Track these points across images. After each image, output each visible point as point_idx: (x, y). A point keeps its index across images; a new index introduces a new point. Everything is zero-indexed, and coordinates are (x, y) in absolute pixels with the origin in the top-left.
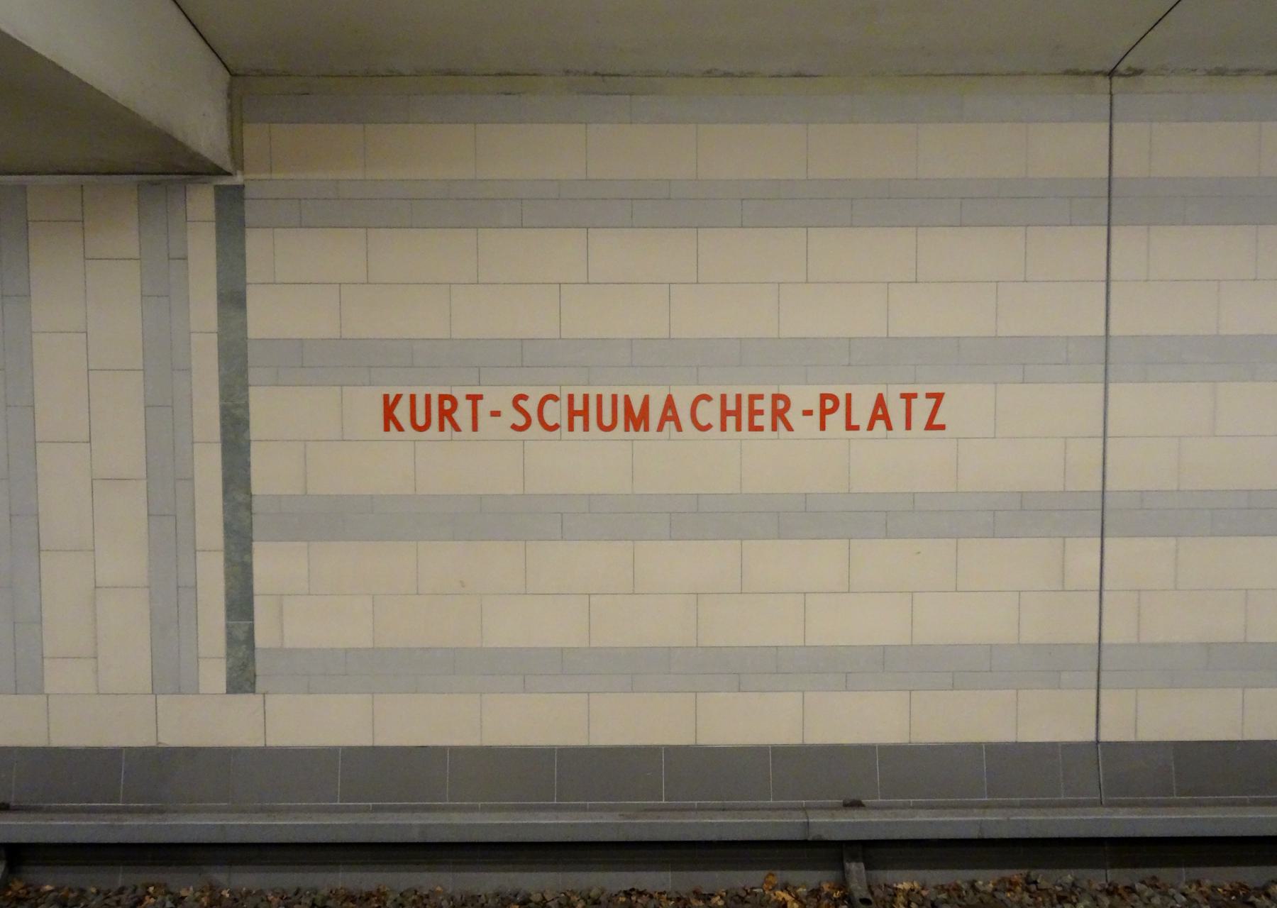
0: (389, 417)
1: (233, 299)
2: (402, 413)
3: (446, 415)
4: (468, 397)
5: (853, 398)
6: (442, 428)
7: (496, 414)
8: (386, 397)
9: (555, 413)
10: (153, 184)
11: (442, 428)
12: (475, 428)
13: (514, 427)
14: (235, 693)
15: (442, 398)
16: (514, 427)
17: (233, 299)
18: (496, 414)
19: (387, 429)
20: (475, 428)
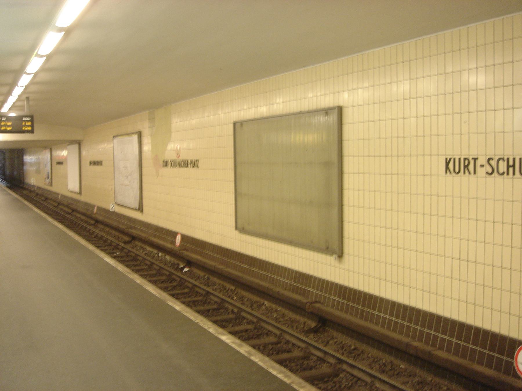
0: (447, 167)
1: (403, 86)
2: (451, 166)
3: (466, 167)
4: (473, 159)
5: (190, 171)
6: (464, 173)
7: (482, 166)
8: (446, 159)
9: (503, 166)
10: (18, 200)
11: (464, 173)
12: (475, 173)
13: (487, 173)
14: (503, 339)
15: (465, 159)
16: (487, 173)
17: (403, 86)
18: (482, 166)
19: (446, 172)
20: (475, 173)
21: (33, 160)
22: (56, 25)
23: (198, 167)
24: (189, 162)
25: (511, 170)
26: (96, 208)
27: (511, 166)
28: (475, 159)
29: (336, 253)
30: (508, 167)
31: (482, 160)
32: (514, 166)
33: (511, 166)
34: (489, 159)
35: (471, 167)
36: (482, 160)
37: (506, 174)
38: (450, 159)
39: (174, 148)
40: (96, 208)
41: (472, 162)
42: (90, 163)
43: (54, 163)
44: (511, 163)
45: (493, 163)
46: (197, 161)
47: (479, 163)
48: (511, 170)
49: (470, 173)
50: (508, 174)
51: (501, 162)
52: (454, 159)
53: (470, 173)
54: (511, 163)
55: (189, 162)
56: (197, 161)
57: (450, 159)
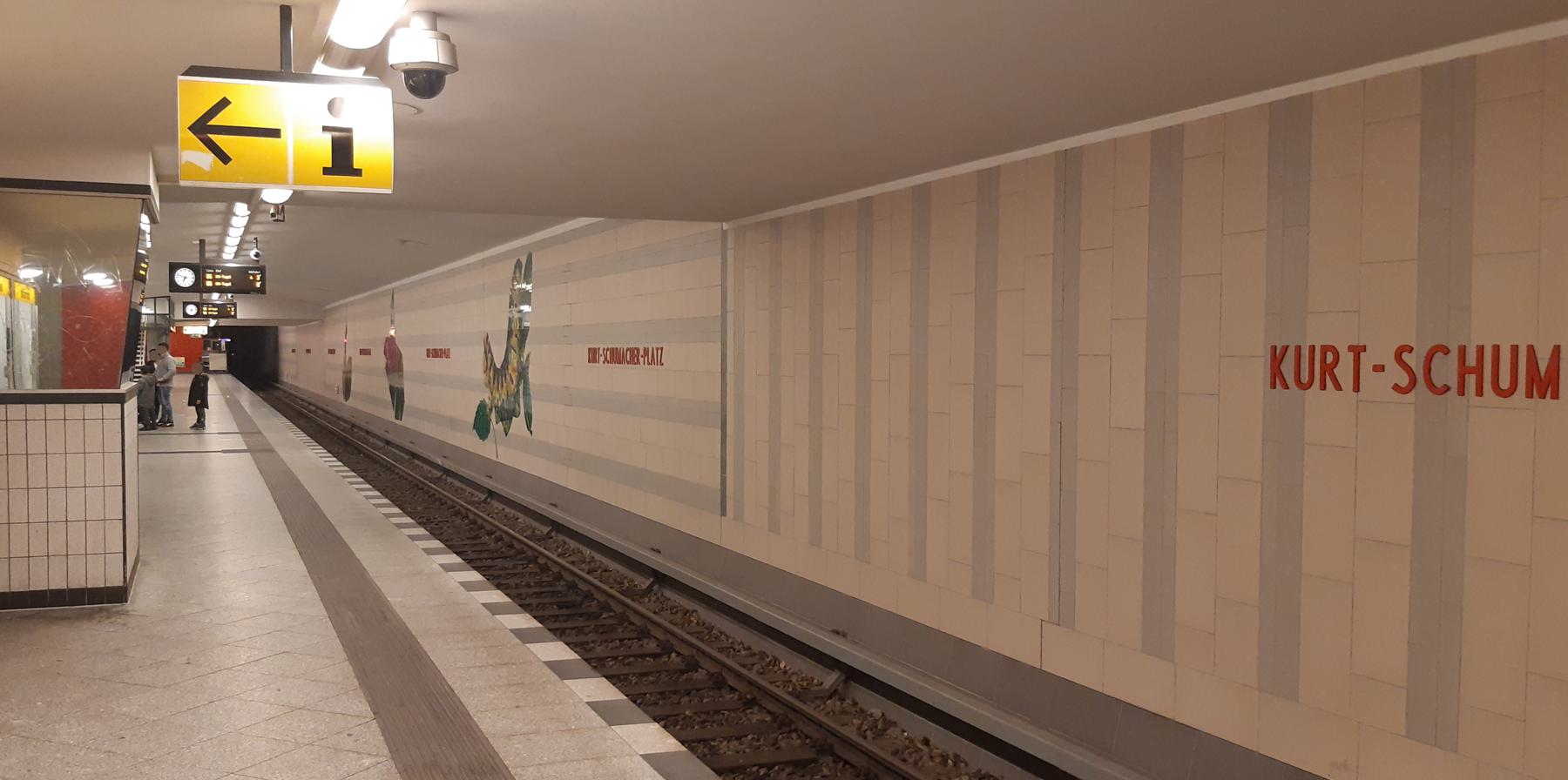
2: (1288, 368)
3: (1329, 370)
4: (1351, 348)
6: (1323, 387)
7: (1379, 368)
9: (1445, 372)
12: (1357, 388)
13: (1396, 388)
15: (1325, 349)
16: (1396, 388)
18: (1379, 368)
19: (1273, 386)
20: (1357, 388)
22: (391, 62)
25: (1471, 380)
27: (1471, 371)
28: (1357, 351)
29: (362, 64)
30: (1463, 371)
31: (1380, 352)
33: (1471, 371)
35: (1344, 372)
36: (1380, 352)
38: (1286, 348)
39: (213, 387)
41: (1347, 359)
42: (593, 355)
44: (1471, 361)
47: (1367, 361)
48: (1471, 380)
49: (1338, 387)
50: (1462, 392)
52: (1298, 349)
53: (1338, 387)
54: (1471, 361)
57: (1286, 348)
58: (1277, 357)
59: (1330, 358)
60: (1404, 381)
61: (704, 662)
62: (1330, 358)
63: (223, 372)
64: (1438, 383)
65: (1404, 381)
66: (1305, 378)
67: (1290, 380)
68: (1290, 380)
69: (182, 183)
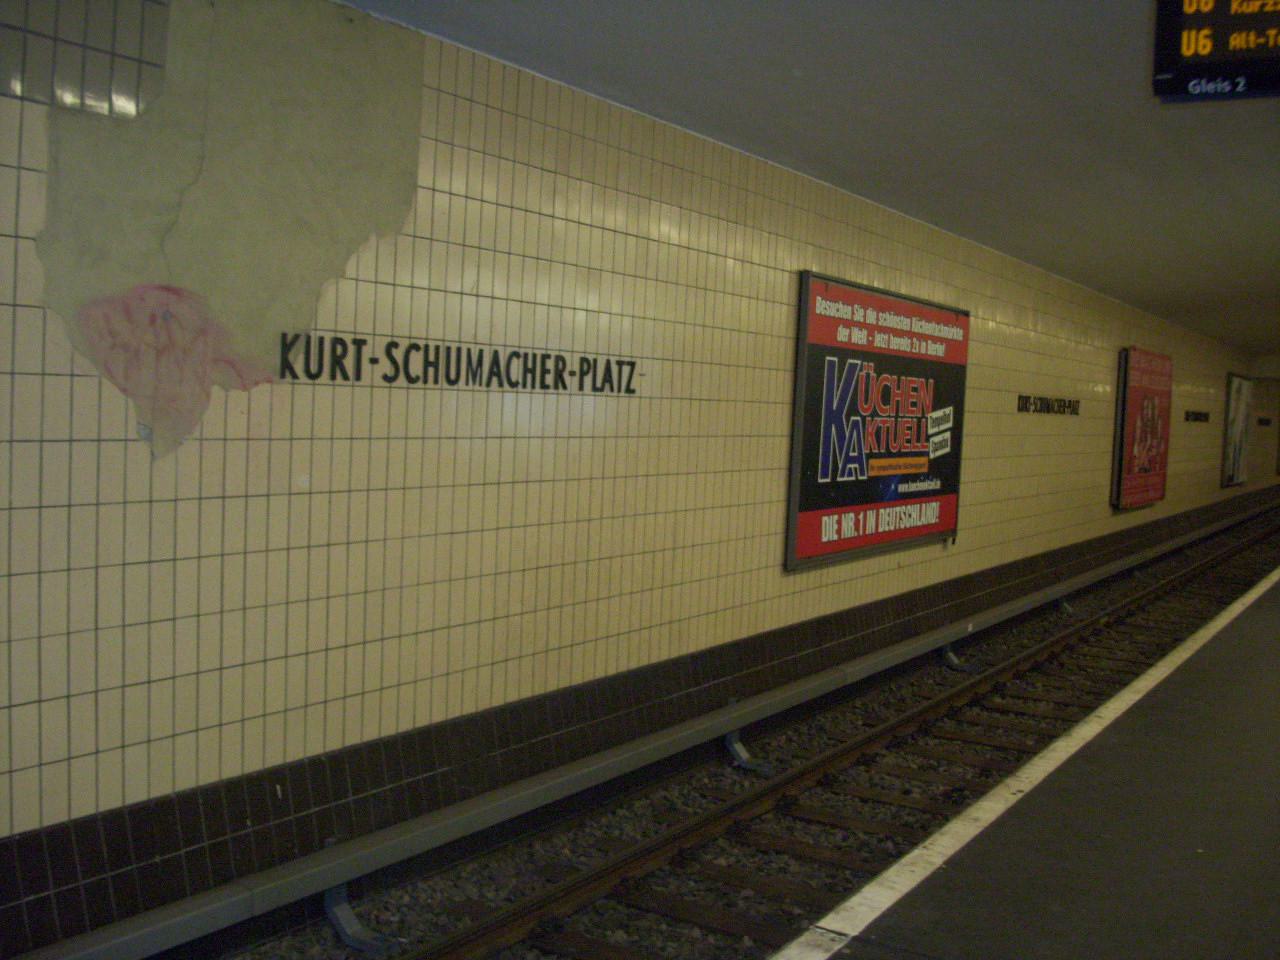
3: (337, 362)
6: (333, 377)
11: (333, 377)
12: (358, 377)
13: (386, 378)
21: (453, 186)
23: (1077, 414)
24: (573, 363)
25: (431, 370)
26: (1160, 77)
28: (359, 344)
32: (436, 365)
34: (393, 345)
35: (349, 363)
37: (520, 387)
38: (297, 337)
40: (1160, 77)
41: (351, 349)
42: (1024, 404)
43: (1216, 418)
45: (398, 354)
46: (1078, 402)
48: (431, 370)
49: (346, 377)
50: (524, 386)
51: (515, 361)
55: (573, 363)
56: (1078, 402)
58: (287, 345)
59: (339, 350)
60: (390, 372)
61: (1001, 680)
62: (339, 350)
63: (249, 393)
64: (514, 379)
65: (390, 372)
66: (314, 369)
67: (299, 367)
68: (299, 367)
69: (1185, 35)
